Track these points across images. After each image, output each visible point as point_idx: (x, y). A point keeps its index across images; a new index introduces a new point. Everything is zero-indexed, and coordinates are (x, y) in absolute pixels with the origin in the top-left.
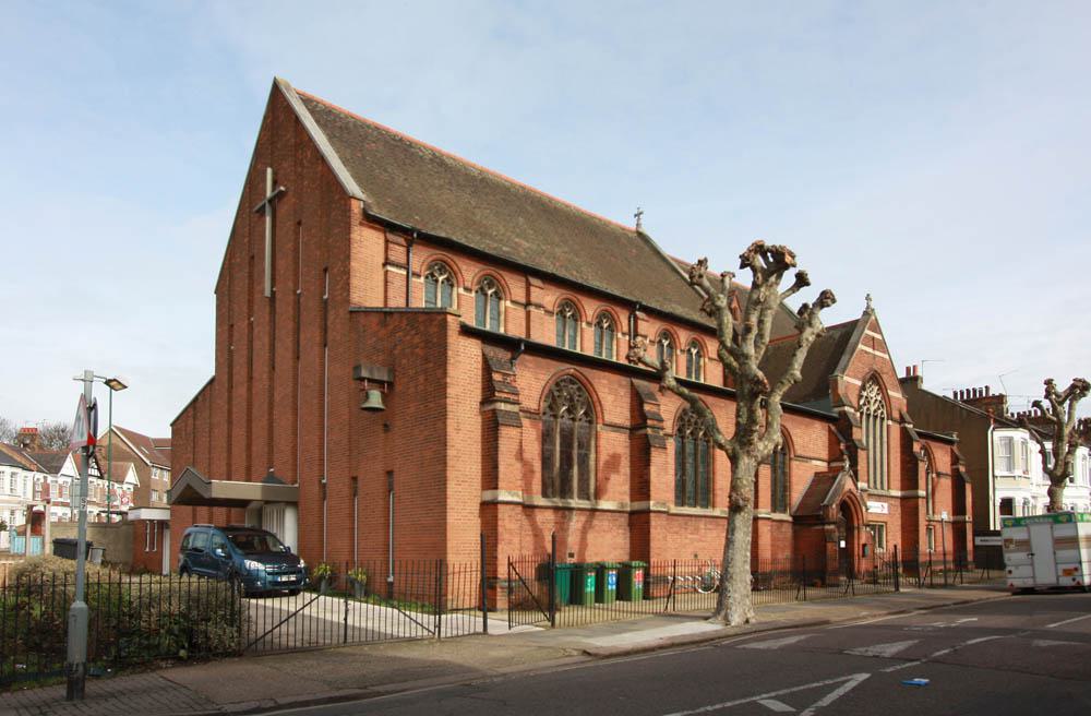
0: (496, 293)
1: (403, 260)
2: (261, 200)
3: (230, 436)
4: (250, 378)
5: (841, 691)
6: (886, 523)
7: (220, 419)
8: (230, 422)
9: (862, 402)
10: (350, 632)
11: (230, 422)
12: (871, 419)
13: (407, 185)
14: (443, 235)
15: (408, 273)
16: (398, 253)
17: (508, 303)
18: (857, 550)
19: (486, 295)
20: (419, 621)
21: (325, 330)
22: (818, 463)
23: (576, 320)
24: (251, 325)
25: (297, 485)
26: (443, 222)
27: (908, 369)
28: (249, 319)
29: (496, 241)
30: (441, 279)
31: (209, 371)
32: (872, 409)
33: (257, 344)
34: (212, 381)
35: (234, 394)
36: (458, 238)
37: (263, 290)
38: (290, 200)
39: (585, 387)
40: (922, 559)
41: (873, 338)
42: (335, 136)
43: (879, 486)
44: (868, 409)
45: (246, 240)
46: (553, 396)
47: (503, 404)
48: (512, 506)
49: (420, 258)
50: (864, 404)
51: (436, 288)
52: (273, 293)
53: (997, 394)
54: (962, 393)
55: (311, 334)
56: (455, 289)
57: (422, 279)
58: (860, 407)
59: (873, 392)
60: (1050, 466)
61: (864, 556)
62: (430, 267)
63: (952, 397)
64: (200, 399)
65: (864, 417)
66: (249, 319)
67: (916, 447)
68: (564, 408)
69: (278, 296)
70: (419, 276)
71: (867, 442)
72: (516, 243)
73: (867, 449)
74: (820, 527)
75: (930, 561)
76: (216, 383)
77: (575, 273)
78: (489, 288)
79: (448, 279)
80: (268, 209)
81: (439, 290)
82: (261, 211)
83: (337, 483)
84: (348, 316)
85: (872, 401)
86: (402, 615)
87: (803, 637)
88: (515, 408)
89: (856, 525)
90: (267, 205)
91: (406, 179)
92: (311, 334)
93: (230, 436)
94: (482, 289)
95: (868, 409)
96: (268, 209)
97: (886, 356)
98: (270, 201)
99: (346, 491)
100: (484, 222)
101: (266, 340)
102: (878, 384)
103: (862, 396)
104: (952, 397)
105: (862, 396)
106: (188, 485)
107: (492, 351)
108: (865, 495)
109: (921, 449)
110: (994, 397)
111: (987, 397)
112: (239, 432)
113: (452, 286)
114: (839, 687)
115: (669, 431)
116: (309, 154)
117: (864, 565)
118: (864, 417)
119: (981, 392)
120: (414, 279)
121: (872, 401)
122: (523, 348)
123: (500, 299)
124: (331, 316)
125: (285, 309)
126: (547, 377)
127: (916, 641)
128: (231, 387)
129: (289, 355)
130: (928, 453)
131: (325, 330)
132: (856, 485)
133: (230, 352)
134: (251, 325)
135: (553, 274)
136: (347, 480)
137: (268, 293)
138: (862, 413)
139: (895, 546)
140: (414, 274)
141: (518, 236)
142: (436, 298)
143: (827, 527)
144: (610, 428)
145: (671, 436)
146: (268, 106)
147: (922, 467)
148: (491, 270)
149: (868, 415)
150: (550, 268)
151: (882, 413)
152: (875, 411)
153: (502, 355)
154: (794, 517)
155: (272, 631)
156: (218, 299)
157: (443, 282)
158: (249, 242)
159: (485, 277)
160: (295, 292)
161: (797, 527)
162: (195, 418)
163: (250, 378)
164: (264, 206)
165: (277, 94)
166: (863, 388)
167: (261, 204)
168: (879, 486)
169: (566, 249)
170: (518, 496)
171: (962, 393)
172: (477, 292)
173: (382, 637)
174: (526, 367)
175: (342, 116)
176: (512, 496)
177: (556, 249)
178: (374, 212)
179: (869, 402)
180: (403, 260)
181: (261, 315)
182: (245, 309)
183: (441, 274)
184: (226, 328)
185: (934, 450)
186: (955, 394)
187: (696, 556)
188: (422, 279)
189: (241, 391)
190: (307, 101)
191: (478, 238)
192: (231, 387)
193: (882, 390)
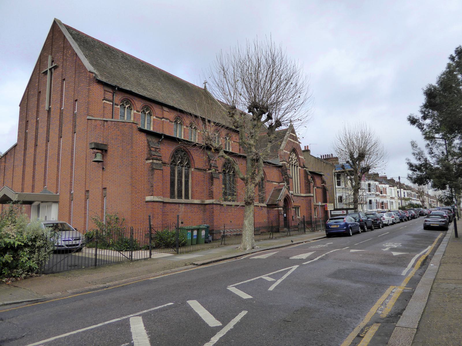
0: (149, 113)
1: (111, 99)
2: (46, 68)
3: (24, 172)
4: (36, 145)
5: (289, 273)
6: (300, 206)
7: (19, 163)
8: (24, 164)
9: (290, 160)
10: (98, 261)
11: (24, 164)
12: (296, 166)
13: (112, 67)
14: (128, 89)
15: (113, 103)
16: (109, 95)
17: (155, 117)
18: (290, 218)
19: (145, 113)
20: (124, 254)
21: (74, 126)
22: (275, 183)
23: (182, 125)
24: (37, 122)
25: (59, 194)
26: (128, 83)
27: (305, 147)
28: (37, 119)
29: (150, 92)
30: (127, 106)
31: (14, 140)
32: (294, 163)
33: (40, 131)
34: (15, 146)
35: (27, 152)
36: (134, 90)
37: (45, 106)
38: (60, 70)
39: (187, 153)
40: (313, 220)
41: (293, 136)
42: (81, 45)
43: (297, 192)
44: (292, 163)
45: (37, 84)
46: (175, 157)
47: (155, 161)
48: (158, 203)
49: (118, 98)
50: (291, 161)
51: (124, 111)
52: (50, 108)
53: (335, 157)
54: (324, 156)
55: (67, 127)
56: (132, 111)
57: (119, 107)
58: (289, 162)
59: (294, 156)
60: (354, 184)
61: (293, 220)
62: (122, 101)
63: (320, 158)
64: (9, 153)
65: (291, 165)
66: (37, 119)
67: (309, 177)
68: (179, 162)
69: (52, 110)
70: (118, 105)
71: (292, 175)
72: (158, 93)
73: (292, 178)
74: (277, 209)
75: (272, 226)
76: (17, 148)
77: (181, 106)
78: (147, 111)
79: (129, 107)
80: (49, 72)
81: (126, 111)
82: (46, 73)
83: (79, 194)
84: (86, 121)
85: (294, 159)
86: (119, 253)
87: (275, 253)
88: (160, 162)
89: (290, 208)
90: (48, 71)
91: (111, 65)
92: (67, 127)
93: (24, 172)
94: (144, 111)
95: (292, 163)
96: (49, 72)
97: (294, 135)
98: (50, 69)
99: (83, 197)
100: (145, 84)
101: (45, 129)
102: (295, 153)
103: (290, 158)
104: (320, 158)
105: (290, 158)
106: (5, 194)
107: (150, 139)
108: (292, 196)
109: (311, 178)
110: (334, 158)
111: (332, 158)
112: (29, 170)
113: (131, 109)
114: (289, 270)
115: (220, 171)
116: (70, 51)
117: (293, 224)
118: (291, 165)
119: (330, 156)
120: (115, 106)
121: (294, 159)
122: (163, 137)
123: (151, 115)
124: (78, 120)
125: (55, 116)
126: (172, 149)
127: (313, 252)
128: (25, 149)
129: (57, 136)
130: (314, 179)
131: (74, 126)
132: (289, 192)
133: (26, 133)
134: (37, 122)
135: (173, 106)
136: (84, 192)
137: (47, 108)
138: (290, 164)
139: (304, 216)
140: (115, 104)
141: (158, 90)
142: (124, 114)
143: (279, 209)
144: (197, 170)
145: (221, 173)
146: (51, 29)
147: (312, 184)
148: (148, 103)
149: (292, 165)
150: (171, 104)
151: (297, 164)
152: (295, 163)
153: (154, 140)
154: (267, 205)
155: (60, 262)
156: (20, 109)
157: (127, 108)
158: (38, 85)
159: (145, 106)
160: (61, 109)
161: (269, 209)
162: (5, 162)
163: (36, 145)
164: (47, 70)
165: (56, 26)
166: (290, 154)
167: (46, 70)
168: (297, 192)
169: (177, 96)
170: (161, 198)
171: (324, 156)
172: (142, 112)
173: (108, 262)
174: (164, 145)
175: (84, 36)
176: (159, 198)
177: (174, 96)
178: (99, 78)
179: (292, 160)
180: (111, 99)
181: (43, 117)
182: (35, 114)
183: (127, 105)
184: (24, 122)
185: (315, 178)
186: (321, 156)
187: (231, 222)
188: (119, 107)
189: (30, 151)
190: (68, 28)
191: (143, 91)
192: (25, 149)
193: (297, 155)
